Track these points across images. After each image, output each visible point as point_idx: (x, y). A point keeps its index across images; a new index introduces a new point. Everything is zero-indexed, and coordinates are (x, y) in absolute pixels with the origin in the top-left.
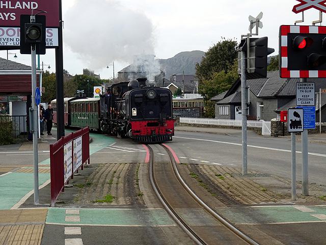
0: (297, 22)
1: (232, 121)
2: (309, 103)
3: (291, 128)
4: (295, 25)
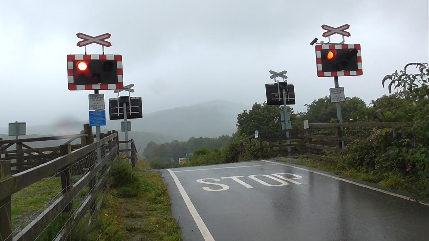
2: (341, 100)
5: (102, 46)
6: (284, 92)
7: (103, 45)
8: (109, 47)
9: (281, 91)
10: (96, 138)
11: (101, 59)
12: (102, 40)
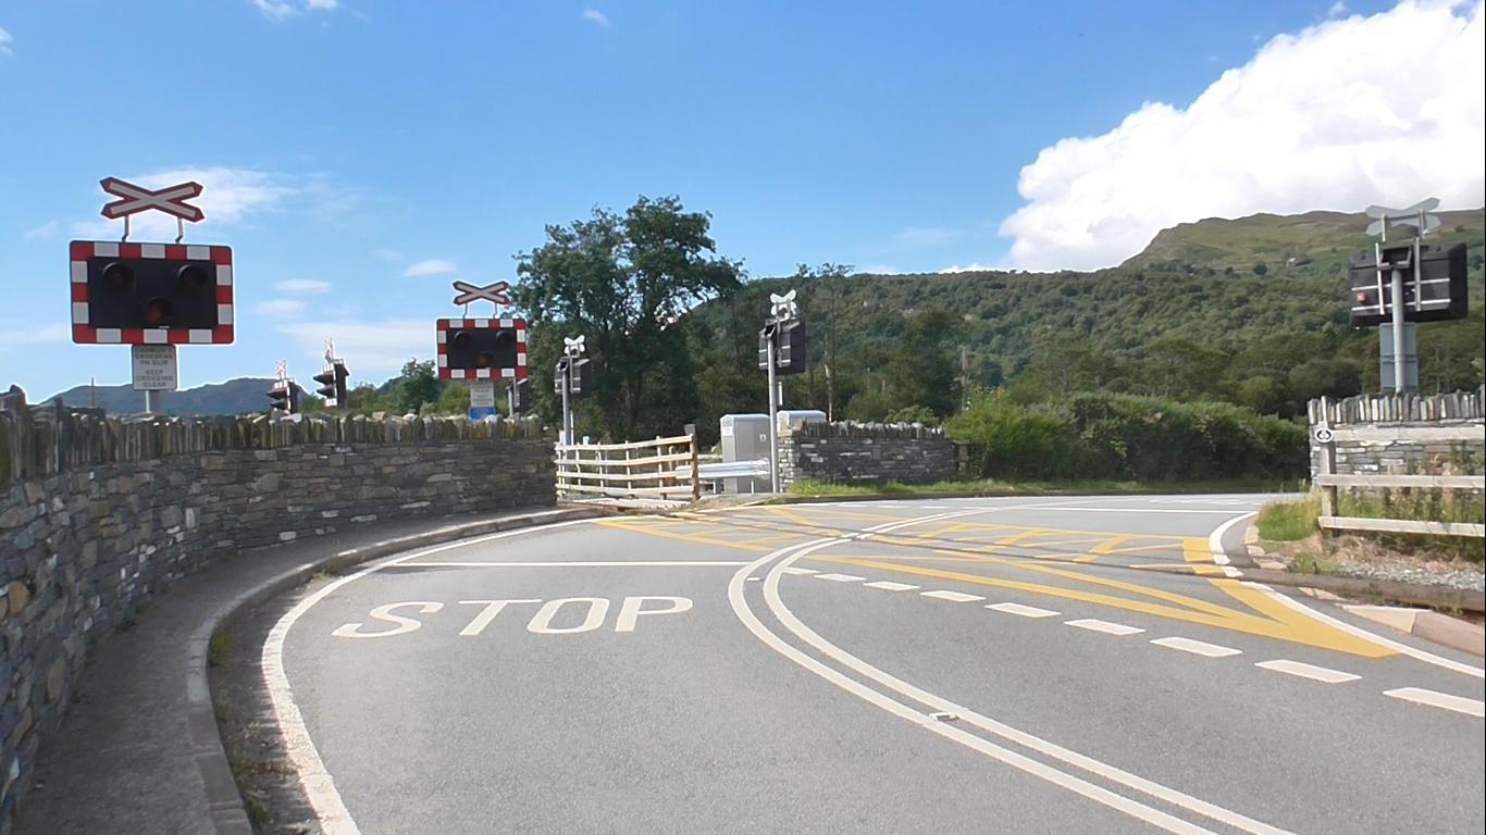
2: (164, 384)
5: (176, 218)
7: (180, 216)
12: (177, 201)
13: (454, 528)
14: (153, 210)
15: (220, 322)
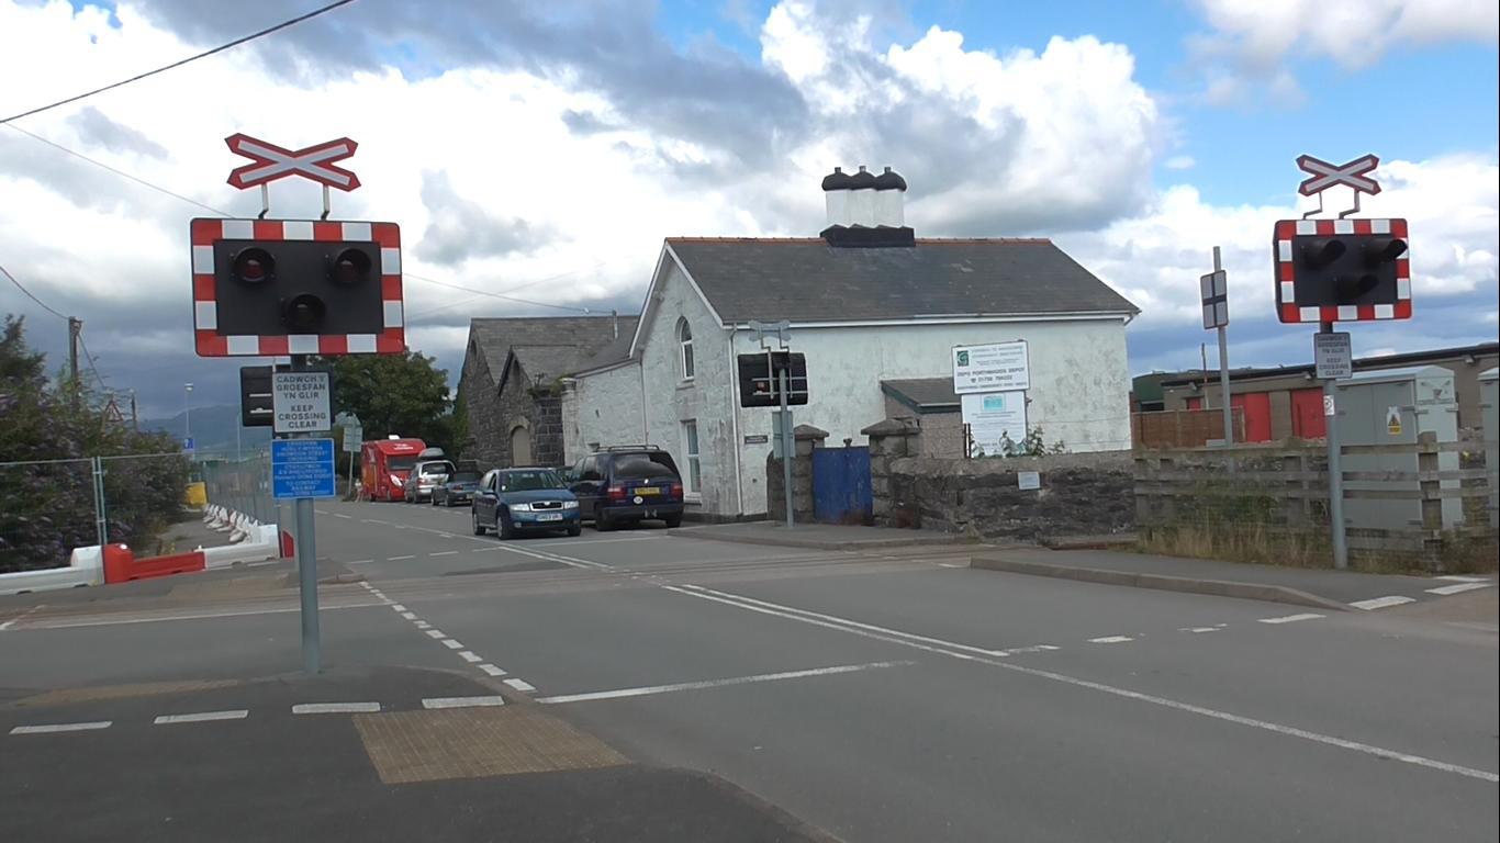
0: (1306, 215)
1: (1227, 378)
2: (314, 424)
3: (423, 472)
4: (1304, 219)
5: (321, 185)
6: (783, 378)
7: (326, 183)
8: (244, 190)
9: (776, 374)
10: (1441, 482)
11: (259, 238)
13: (957, 655)
14: (295, 176)
15: (1400, 297)
